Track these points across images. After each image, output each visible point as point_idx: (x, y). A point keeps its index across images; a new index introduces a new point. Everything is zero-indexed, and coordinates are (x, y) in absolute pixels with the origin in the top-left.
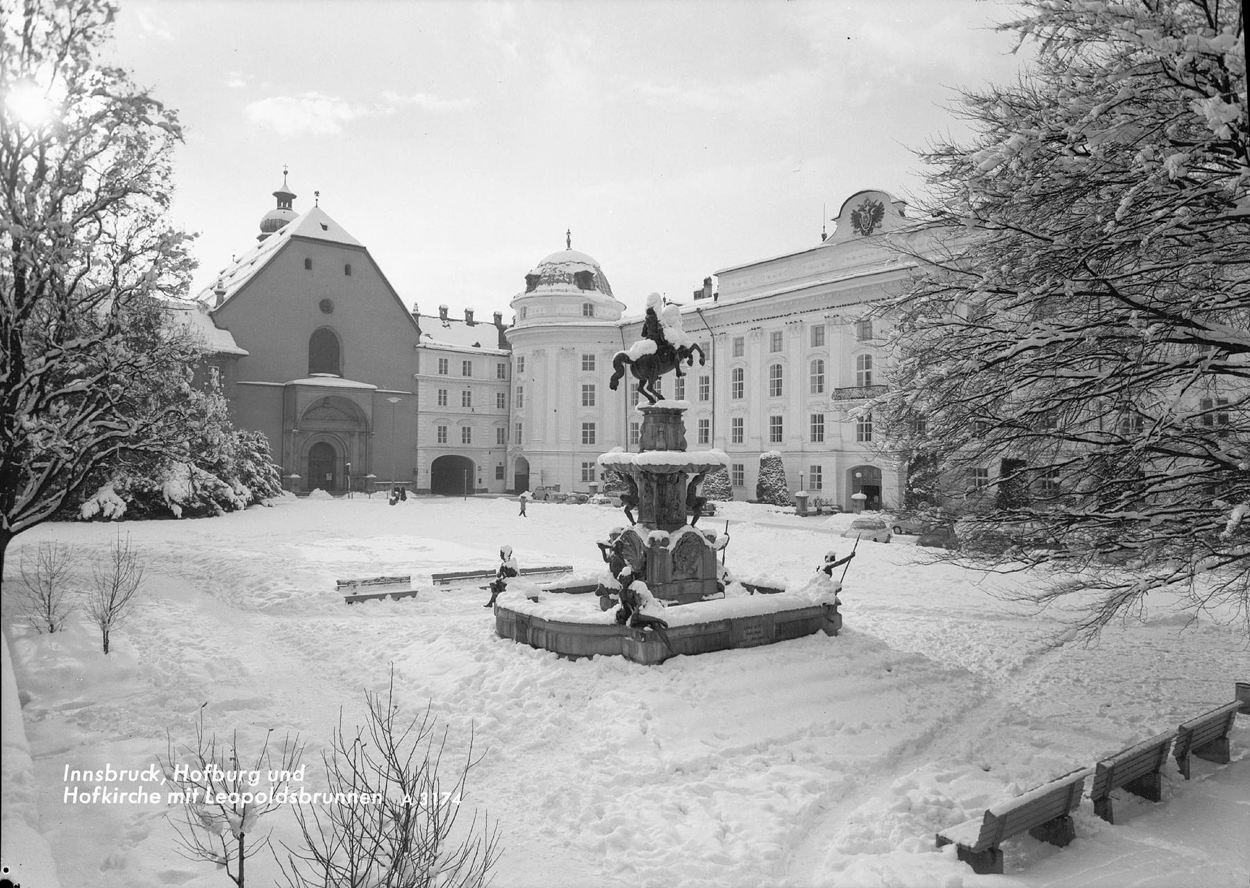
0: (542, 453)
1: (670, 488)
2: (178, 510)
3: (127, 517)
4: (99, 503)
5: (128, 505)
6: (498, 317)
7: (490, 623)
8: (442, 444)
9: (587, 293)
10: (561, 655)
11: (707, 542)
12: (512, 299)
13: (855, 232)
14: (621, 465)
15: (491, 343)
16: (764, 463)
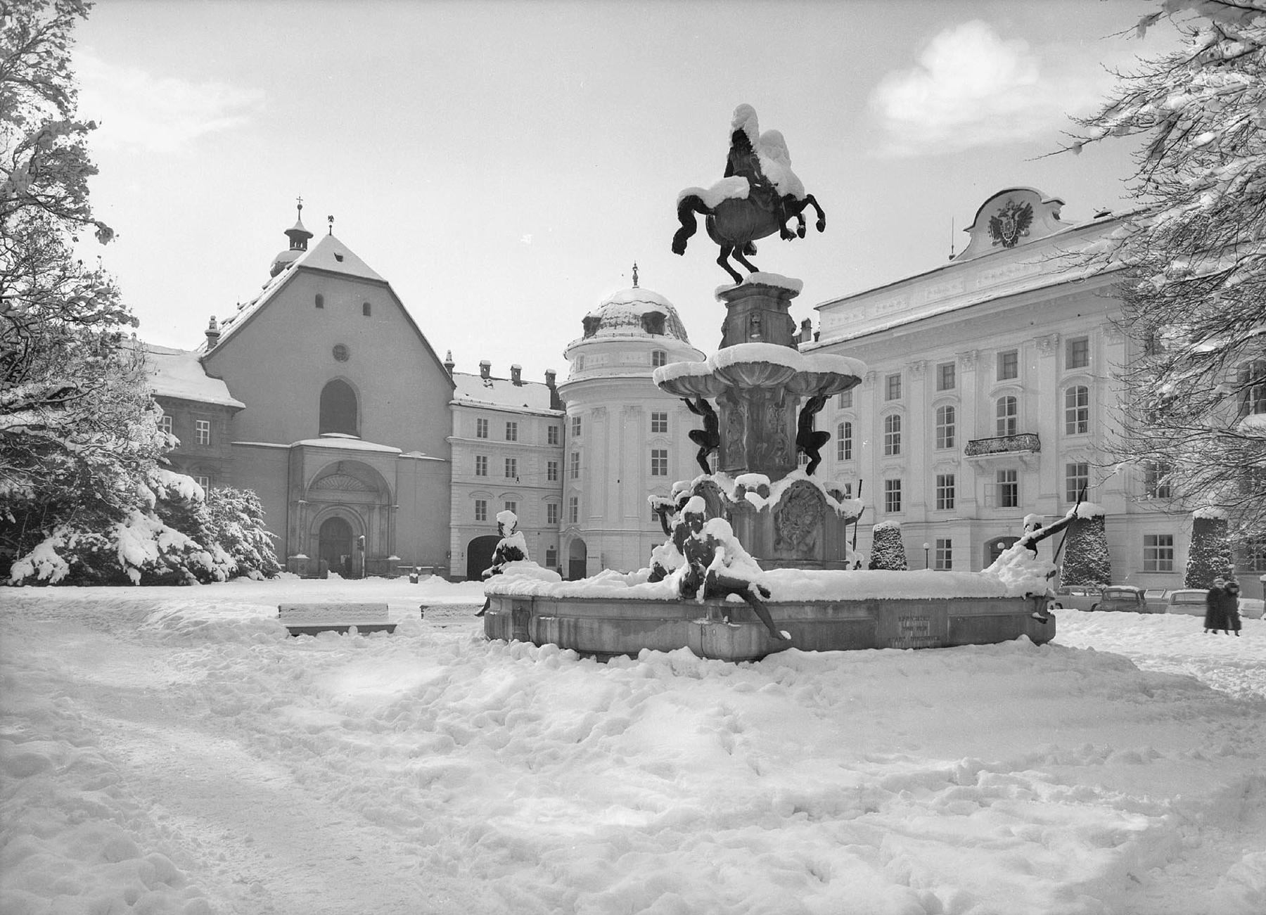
0: (603, 533)
1: (770, 413)
2: (135, 576)
3: (66, 582)
4: (33, 564)
5: (71, 567)
6: (551, 376)
7: (479, 629)
8: (481, 522)
9: (658, 338)
10: (583, 653)
11: (831, 500)
12: (566, 347)
13: (995, 244)
14: (690, 378)
15: (542, 403)
16: (878, 536)
